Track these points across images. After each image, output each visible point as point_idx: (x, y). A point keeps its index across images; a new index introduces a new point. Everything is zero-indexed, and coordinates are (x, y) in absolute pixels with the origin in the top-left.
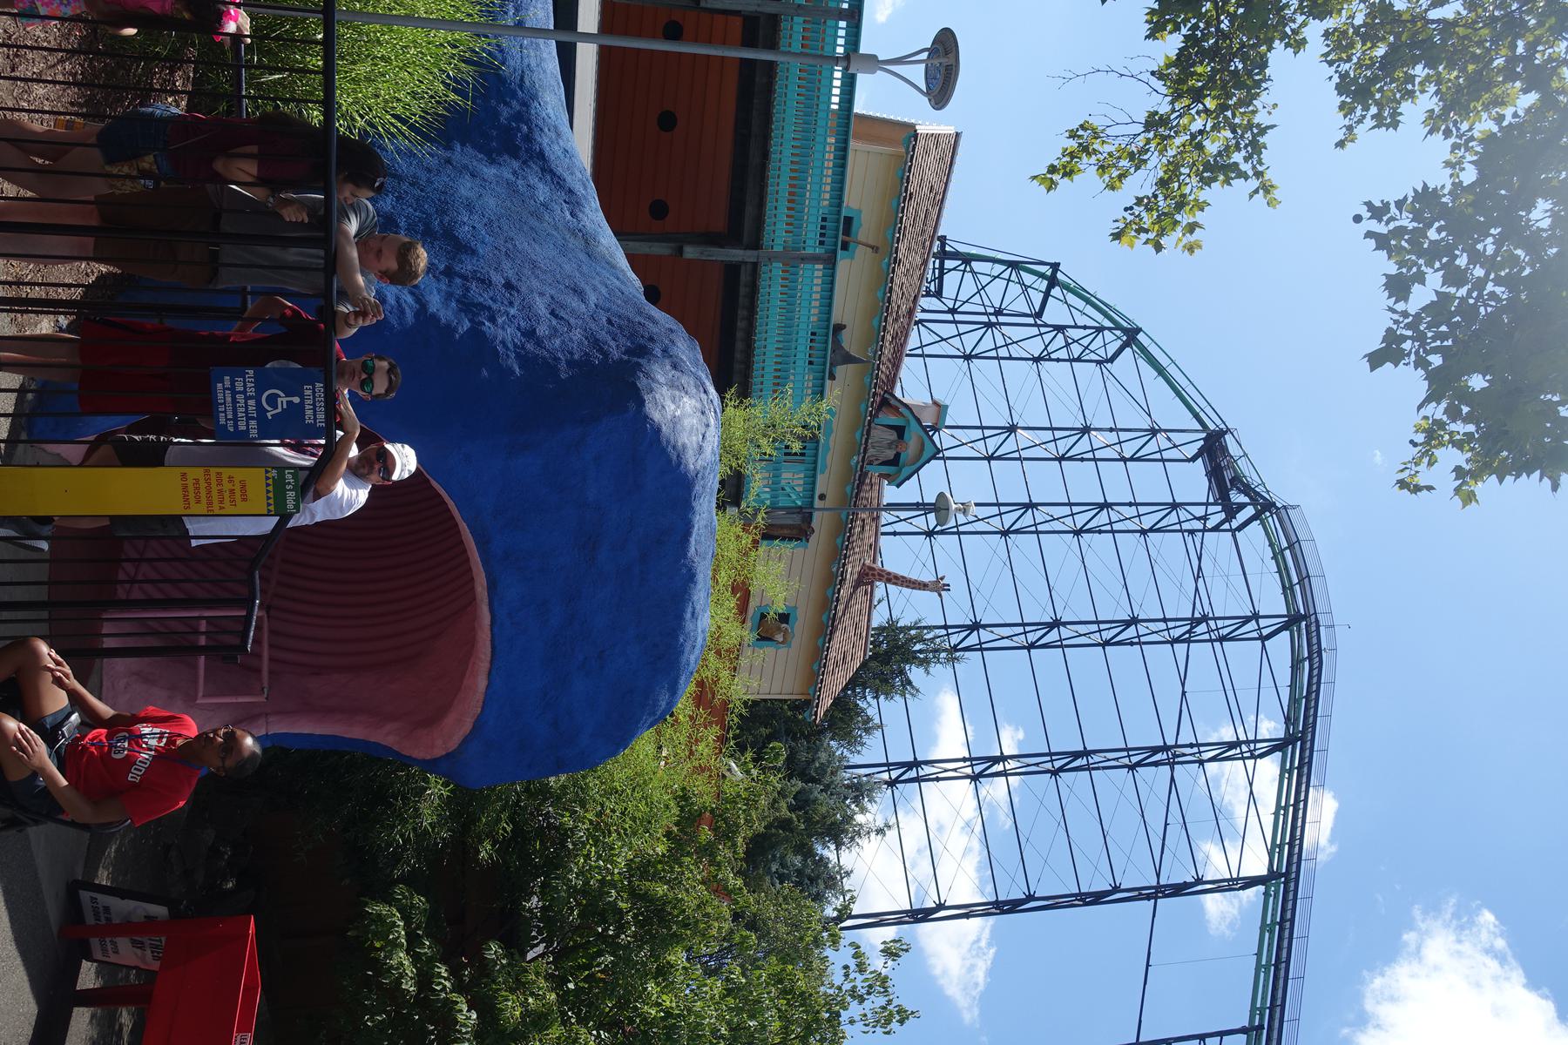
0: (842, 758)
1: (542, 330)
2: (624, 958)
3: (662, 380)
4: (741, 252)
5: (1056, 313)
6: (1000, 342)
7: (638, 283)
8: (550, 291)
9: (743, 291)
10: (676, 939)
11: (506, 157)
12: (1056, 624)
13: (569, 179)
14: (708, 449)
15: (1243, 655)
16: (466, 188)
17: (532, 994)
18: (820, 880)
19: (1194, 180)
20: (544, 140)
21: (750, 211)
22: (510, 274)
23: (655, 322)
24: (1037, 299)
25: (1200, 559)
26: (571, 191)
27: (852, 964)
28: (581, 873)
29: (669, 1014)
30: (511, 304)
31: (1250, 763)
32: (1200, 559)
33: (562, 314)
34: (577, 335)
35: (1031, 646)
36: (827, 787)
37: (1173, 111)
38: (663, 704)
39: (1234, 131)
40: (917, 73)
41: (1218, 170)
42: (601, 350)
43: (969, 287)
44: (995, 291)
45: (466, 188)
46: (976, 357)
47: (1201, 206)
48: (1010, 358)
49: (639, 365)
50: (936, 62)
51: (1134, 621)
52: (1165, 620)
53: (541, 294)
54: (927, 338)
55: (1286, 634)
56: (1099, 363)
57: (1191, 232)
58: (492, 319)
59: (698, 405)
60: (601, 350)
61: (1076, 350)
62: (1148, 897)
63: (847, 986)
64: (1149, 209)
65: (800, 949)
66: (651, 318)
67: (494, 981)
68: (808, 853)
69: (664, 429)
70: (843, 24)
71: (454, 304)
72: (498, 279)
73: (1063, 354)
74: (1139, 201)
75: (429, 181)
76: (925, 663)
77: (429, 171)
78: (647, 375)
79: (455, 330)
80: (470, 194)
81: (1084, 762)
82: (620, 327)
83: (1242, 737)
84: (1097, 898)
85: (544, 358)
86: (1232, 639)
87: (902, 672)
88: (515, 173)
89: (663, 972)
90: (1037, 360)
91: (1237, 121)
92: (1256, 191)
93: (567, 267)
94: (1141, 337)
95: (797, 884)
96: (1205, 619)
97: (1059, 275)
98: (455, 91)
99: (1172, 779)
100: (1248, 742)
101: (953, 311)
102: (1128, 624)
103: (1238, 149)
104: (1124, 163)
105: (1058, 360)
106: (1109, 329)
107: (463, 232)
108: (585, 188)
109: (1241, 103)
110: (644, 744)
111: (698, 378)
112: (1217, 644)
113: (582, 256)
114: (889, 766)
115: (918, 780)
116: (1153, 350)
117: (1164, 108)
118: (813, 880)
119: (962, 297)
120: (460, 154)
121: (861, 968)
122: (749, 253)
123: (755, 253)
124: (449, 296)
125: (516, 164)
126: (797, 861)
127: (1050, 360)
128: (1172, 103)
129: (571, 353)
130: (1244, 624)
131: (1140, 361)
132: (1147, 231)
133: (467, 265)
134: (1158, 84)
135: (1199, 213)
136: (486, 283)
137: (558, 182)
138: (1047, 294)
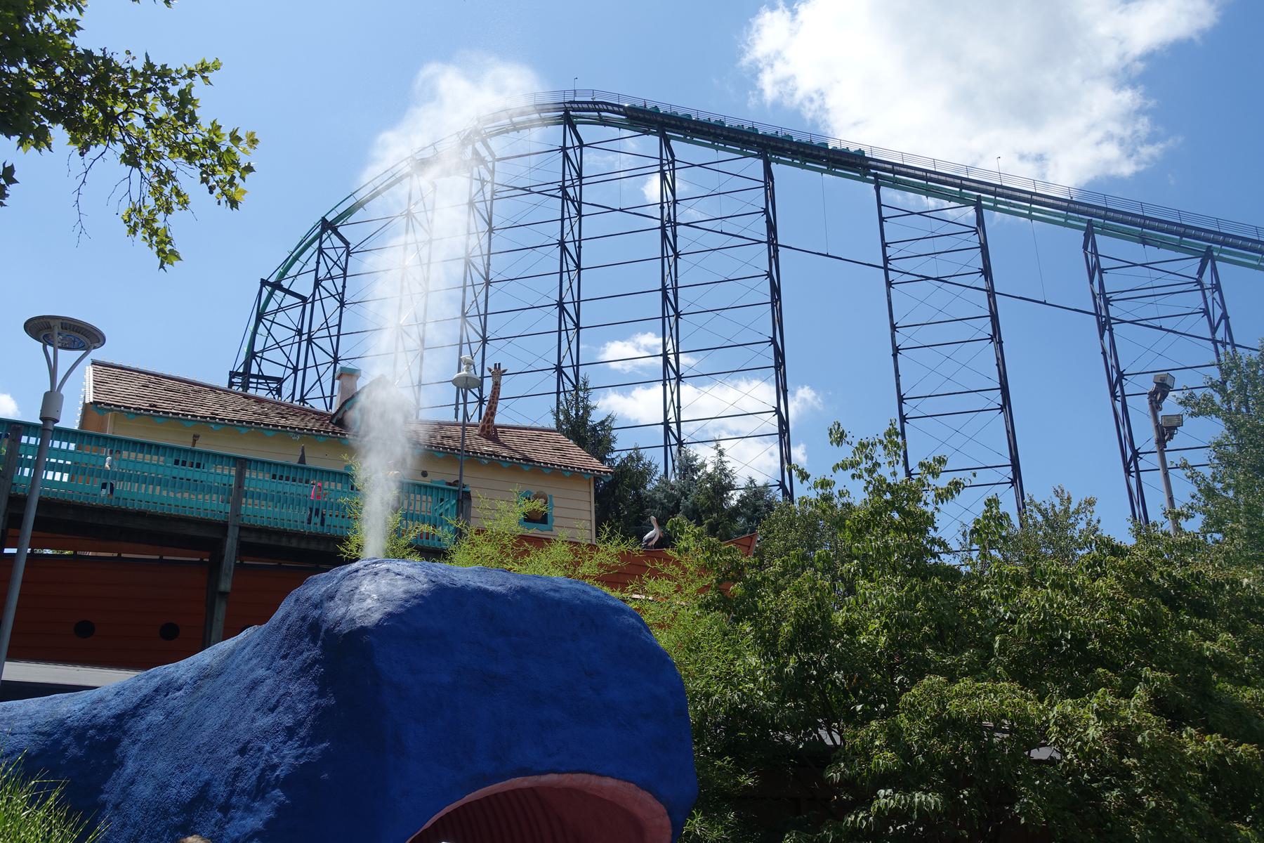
0: (660, 480)
1: (288, 720)
2: (840, 661)
3: (343, 610)
4: (229, 541)
5: (304, 286)
6: (325, 333)
7: (250, 630)
8: (251, 712)
9: (264, 541)
10: (826, 618)
11: (118, 751)
12: (561, 305)
13: (145, 691)
14: (410, 571)
15: (592, 161)
16: (144, 790)
17: (872, 741)
18: (756, 500)
19: (190, 130)
20: (105, 713)
21: (192, 531)
22: (231, 749)
23: (288, 615)
24: (290, 300)
25: (516, 188)
26: (157, 690)
27: (851, 471)
28: (770, 699)
29: (886, 626)
30: (260, 749)
31: (677, 165)
32: (516, 188)
33: (273, 701)
34: (295, 688)
35: (577, 326)
36: (683, 494)
37: (123, 141)
38: (632, 620)
39: (149, 90)
40: (66, 358)
41: (184, 106)
42: (311, 666)
43: (276, 355)
44: (280, 334)
45: (144, 790)
46: (336, 353)
47: (216, 128)
48: (339, 325)
49: (327, 631)
50: (58, 339)
51: (562, 244)
52: (563, 220)
53: (253, 720)
54: (317, 392)
55: (579, 127)
56: (348, 254)
57: (240, 139)
58: (274, 767)
59: (369, 578)
60: (311, 666)
61: (336, 271)
62: (776, 251)
63: (865, 475)
64: (214, 173)
65: (829, 517)
66: (283, 619)
67: (859, 774)
68: (735, 512)
69: (389, 609)
70: (24, 439)
71: (256, 804)
72: (235, 762)
73: (339, 282)
74: (204, 180)
75: (134, 826)
76: (587, 410)
77: (124, 825)
78: (338, 623)
79: (281, 804)
80: (151, 787)
81: (670, 291)
82: (290, 647)
83: (658, 168)
84: (776, 290)
85: (314, 720)
86: (581, 169)
87: (594, 428)
88: (134, 743)
89: (852, 628)
90: (342, 304)
91: (139, 85)
92: (203, 77)
93: (228, 696)
94: (329, 218)
95: (759, 522)
96: (563, 188)
97: (272, 280)
98: (47, 797)
99: (687, 225)
100: (662, 165)
101: (295, 370)
102: (564, 249)
103: (165, 89)
104: (167, 190)
105: (344, 287)
106: (321, 243)
107: (187, 793)
108: (155, 676)
109: (123, 81)
110: (663, 640)
111: (344, 577)
112: (584, 181)
113: (220, 680)
114: (666, 445)
115: (678, 422)
116: (341, 210)
117: (120, 148)
118: (756, 509)
119: (284, 361)
120: (110, 795)
121: (853, 465)
122: (230, 533)
123: (230, 528)
124: (249, 809)
125: (126, 741)
126: (741, 520)
127: (343, 293)
128: (114, 141)
129: (312, 693)
130: (569, 159)
131: (350, 221)
132: (233, 178)
133: (220, 790)
134: (94, 151)
135: (222, 131)
136: (238, 773)
137: (147, 702)
138: (287, 292)
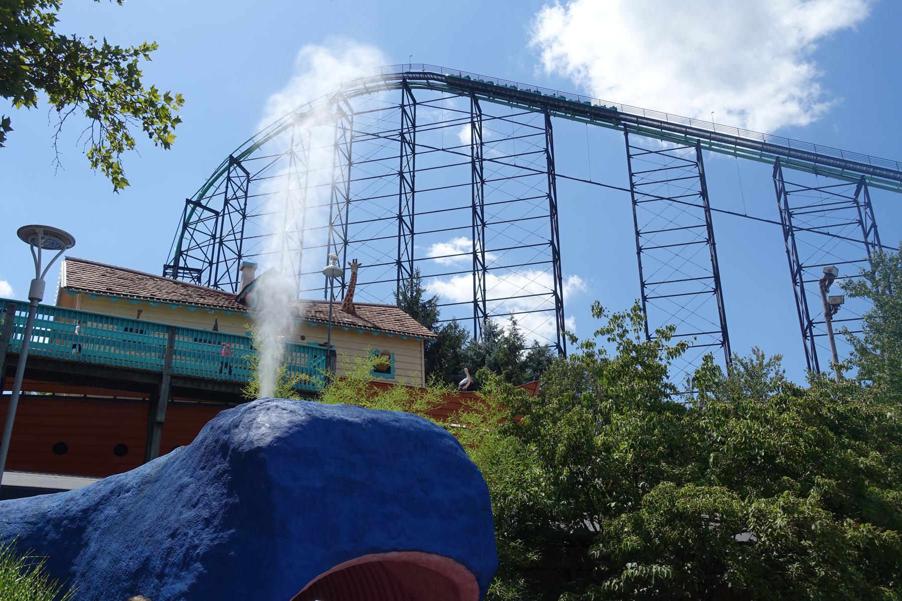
0: (471, 342)
1: (205, 514)
2: (600, 472)
3: (245, 435)
4: (163, 385)
5: (217, 204)
6: (232, 237)
7: (178, 449)
8: (179, 508)
9: (189, 385)
10: (589, 440)
11: (84, 535)
12: (400, 217)
13: (103, 493)
14: (293, 407)
15: (423, 115)
16: (103, 563)
17: (622, 528)
19: (136, 92)
20: (75, 509)
21: (137, 379)
22: (165, 534)
23: (205, 439)
24: (207, 214)
25: (368, 134)
26: (112, 492)
27: (608, 336)
28: (549, 498)
29: (632, 446)
30: (186, 534)
31: (483, 117)
32: (368, 134)
33: (195, 500)
34: (210, 490)
35: (412, 233)
36: (488, 352)
37: (88, 101)
38: (451, 442)
39: (107, 64)
40: (47, 255)
41: (131, 76)
42: (222, 474)
43: (197, 253)
44: (200, 238)
45: (103, 563)
46: (240, 252)
47: (154, 91)
48: (242, 232)
49: (234, 450)
50: (41, 241)
51: (401, 174)
52: (401, 157)
53: (181, 513)
54: (226, 280)
55: (413, 91)
56: (249, 181)
57: (171, 99)
58: (196, 547)
59: (263, 412)
60: (222, 474)
61: (240, 193)
62: (554, 179)
63: (618, 339)
64: (153, 123)
65: (592, 368)
66: (202, 442)
67: (613, 552)
68: (525, 365)
69: (278, 434)
70: (17, 313)
71: (183, 573)
72: (168, 543)
73: (242, 201)
74: (146, 129)
75: (95, 589)
76: (419, 292)
77: (89, 588)
78: (241, 444)
79: (201, 573)
80: (107, 561)
81: (478, 208)
82: (207, 462)
83: (470, 120)
84: (553, 207)
85: (224, 513)
86: (414, 120)
87: (424, 305)
88: (96, 530)
89: (608, 448)
90: (244, 217)
91: (99, 61)
92: (145, 55)
93: (163, 496)
94: (235, 156)
95: (541, 372)
96: (402, 134)
97: (194, 200)
98: (33, 568)
99: (490, 160)
100: (472, 118)
101: (211, 264)
102: (402, 178)
103: (118, 64)
104: (119, 136)
105: (245, 204)
106: (229, 173)
107: (134, 565)
108: (110, 482)
109: (88, 58)
110: (473, 456)
111: (245, 411)
112: (417, 129)
113: (157, 485)
114: (476, 318)
115: (484, 301)
116: (243, 149)
117: (86, 106)
118: (540, 363)
119: (203, 257)
120: (79, 567)
121: (609, 331)
122: (164, 380)
123: (164, 376)
124: (177, 577)
125: (90, 529)
126: (529, 371)
127: (245, 209)
128: (81, 100)
129: (223, 494)
130: (406, 113)
131: (249, 157)
132: (166, 127)
133: (157, 563)
134: (67, 108)
135: (159, 93)
136: (170, 551)
137: (105, 500)
138: (205, 208)
